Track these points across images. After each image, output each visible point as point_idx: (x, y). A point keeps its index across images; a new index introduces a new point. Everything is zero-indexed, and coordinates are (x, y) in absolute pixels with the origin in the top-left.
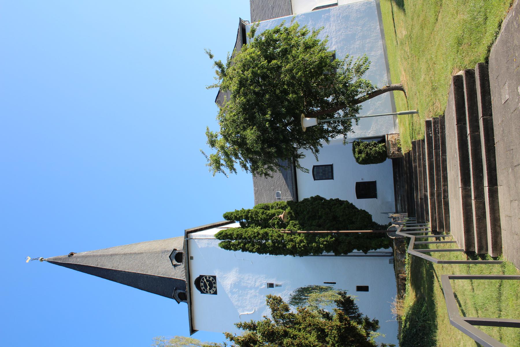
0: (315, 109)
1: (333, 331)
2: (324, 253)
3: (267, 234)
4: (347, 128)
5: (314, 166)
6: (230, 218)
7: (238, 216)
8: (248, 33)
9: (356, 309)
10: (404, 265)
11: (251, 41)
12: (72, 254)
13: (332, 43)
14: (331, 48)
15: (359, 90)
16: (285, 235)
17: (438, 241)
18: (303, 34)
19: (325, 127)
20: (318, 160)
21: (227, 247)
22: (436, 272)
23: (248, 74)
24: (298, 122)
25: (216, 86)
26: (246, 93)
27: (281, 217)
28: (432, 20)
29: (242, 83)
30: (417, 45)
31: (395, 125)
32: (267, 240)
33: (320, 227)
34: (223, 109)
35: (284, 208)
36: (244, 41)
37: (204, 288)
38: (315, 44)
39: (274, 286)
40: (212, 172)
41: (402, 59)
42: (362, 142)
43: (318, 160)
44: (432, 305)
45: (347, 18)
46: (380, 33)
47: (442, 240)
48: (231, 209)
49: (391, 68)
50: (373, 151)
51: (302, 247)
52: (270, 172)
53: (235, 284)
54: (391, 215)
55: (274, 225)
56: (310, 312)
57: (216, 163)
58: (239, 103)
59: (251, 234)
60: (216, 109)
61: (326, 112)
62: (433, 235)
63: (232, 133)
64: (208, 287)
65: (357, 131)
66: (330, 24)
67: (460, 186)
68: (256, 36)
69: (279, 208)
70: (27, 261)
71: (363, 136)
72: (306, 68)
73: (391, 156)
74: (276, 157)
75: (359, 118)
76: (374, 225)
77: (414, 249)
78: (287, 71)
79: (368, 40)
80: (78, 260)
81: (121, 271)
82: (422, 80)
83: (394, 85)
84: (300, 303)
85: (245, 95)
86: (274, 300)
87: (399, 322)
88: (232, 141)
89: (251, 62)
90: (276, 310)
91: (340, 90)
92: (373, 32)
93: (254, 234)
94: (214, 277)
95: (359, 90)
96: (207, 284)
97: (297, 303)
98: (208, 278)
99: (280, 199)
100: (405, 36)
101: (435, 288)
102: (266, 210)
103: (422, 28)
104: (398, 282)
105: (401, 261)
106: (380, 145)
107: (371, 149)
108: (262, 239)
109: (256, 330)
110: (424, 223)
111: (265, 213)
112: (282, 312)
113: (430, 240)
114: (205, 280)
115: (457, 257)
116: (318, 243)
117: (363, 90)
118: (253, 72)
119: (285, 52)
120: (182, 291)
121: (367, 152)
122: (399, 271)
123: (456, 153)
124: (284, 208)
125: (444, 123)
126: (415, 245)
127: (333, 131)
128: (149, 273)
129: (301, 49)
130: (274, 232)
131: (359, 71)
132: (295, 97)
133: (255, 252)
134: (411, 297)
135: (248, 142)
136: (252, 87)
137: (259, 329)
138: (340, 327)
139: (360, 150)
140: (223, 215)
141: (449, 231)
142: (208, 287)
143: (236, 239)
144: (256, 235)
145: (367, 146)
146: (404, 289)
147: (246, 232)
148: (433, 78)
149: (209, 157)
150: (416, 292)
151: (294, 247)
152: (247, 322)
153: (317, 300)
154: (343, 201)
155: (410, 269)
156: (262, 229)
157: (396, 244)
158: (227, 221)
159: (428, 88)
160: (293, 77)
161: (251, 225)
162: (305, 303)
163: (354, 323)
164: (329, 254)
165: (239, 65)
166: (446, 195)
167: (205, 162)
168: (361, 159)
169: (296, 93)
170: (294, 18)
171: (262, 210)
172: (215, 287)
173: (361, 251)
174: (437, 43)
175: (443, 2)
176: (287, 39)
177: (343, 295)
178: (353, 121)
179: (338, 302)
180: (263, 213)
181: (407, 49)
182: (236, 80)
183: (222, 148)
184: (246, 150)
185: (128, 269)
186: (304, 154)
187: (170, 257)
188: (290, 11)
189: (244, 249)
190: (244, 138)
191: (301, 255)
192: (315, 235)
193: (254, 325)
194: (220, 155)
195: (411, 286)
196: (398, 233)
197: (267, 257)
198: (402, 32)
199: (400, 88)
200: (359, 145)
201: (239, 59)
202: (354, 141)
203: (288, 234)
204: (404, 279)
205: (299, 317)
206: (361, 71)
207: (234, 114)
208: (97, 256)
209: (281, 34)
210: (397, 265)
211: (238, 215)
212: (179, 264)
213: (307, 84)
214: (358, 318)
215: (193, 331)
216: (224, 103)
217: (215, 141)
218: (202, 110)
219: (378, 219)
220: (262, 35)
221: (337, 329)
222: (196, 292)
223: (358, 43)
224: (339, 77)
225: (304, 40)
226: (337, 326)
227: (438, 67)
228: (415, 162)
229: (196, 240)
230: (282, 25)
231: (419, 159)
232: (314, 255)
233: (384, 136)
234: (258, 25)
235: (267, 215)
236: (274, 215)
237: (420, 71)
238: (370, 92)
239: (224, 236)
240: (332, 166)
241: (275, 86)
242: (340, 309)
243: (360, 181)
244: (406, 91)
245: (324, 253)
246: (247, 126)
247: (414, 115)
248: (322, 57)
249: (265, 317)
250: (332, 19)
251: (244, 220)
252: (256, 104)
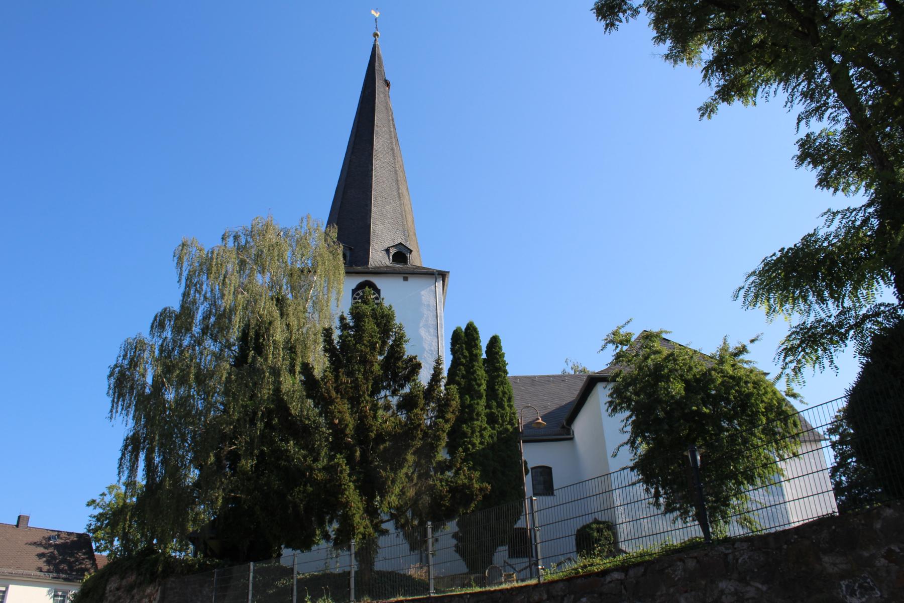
21: (456, 337)
70: (373, 12)
80: (382, 96)
81: (372, 164)
151: (465, 435)
222: (355, 281)
229: (433, 287)
235: (502, 400)
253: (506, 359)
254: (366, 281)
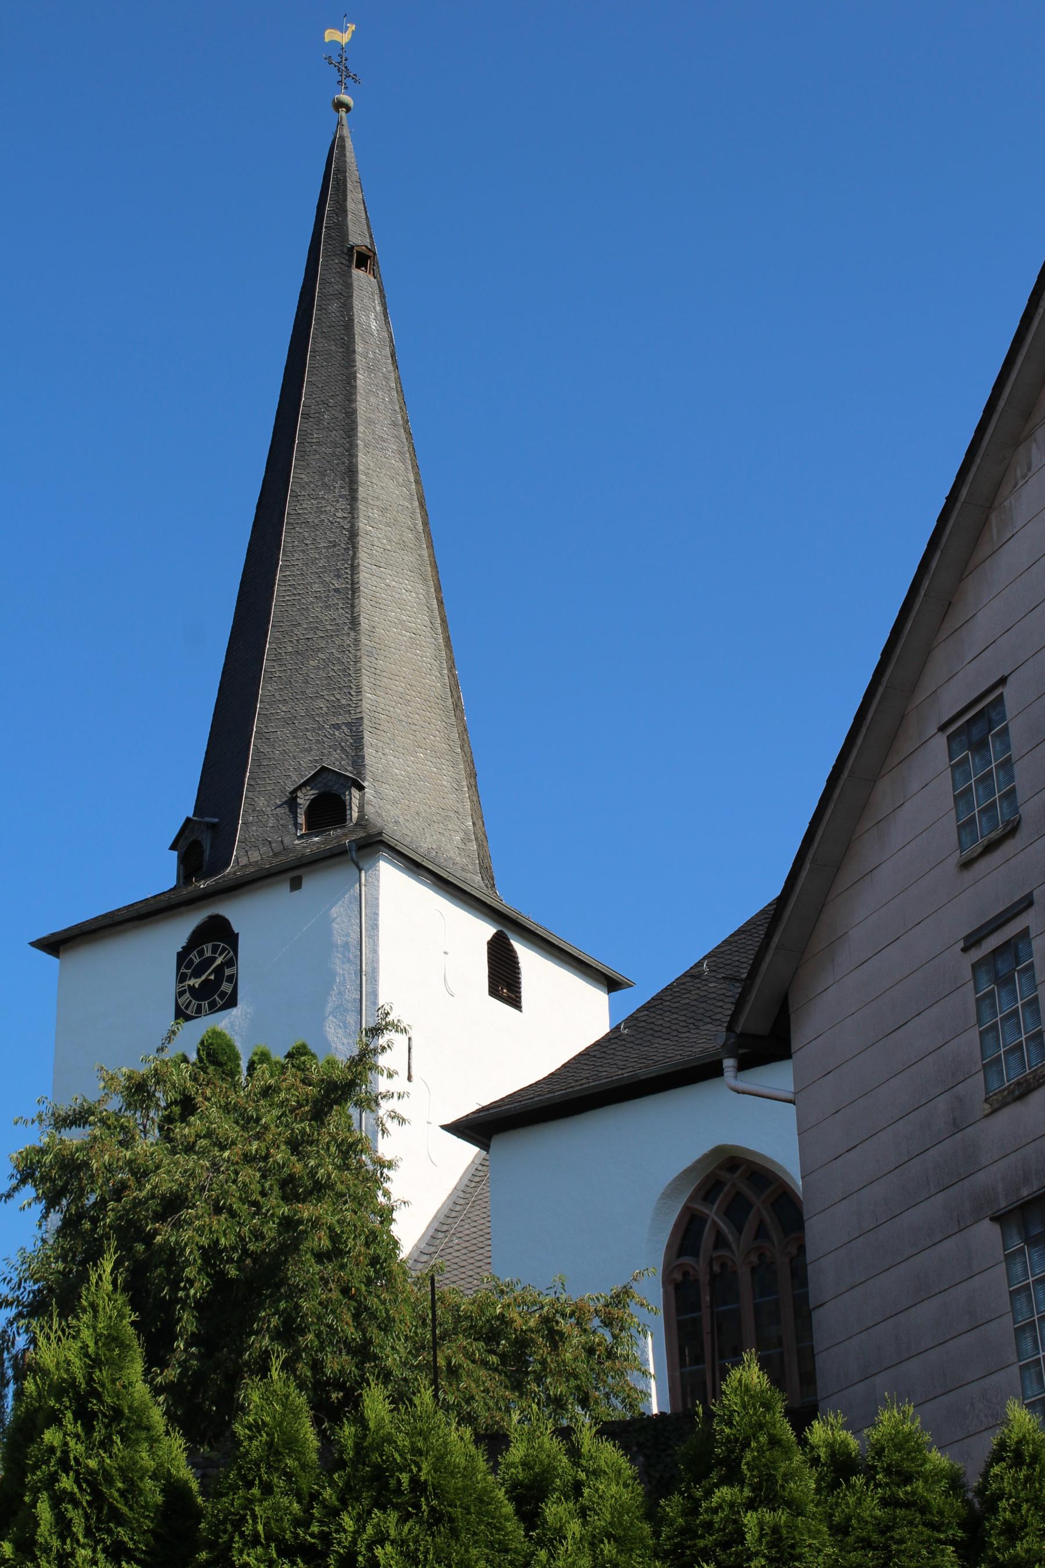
37: (197, 961)
98: (228, 972)
172: (199, 1010)
175: (585, 1562)
185: (285, 580)
212: (302, 819)
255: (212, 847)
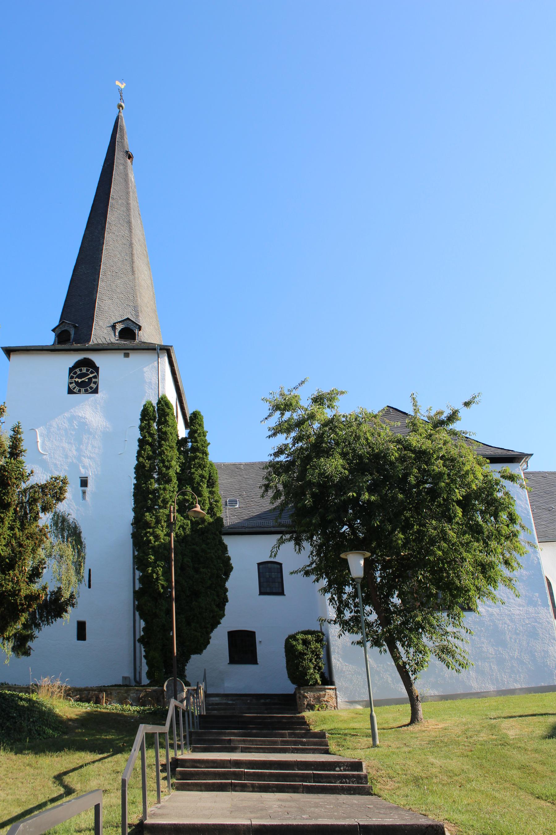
0: (378, 574)
1: (10, 584)
2: (138, 574)
3: (169, 481)
4: (346, 625)
5: (280, 564)
6: (193, 421)
7: (196, 435)
8: (509, 468)
9: (48, 621)
10: (121, 702)
11: (495, 471)
12: (130, 157)
13: (490, 606)
14: (483, 607)
15: (412, 650)
16: (167, 512)
17: (160, 768)
18: (507, 563)
19: (348, 589)
20: (291, 573)
21: (145, 414)
22: (110, 759)
23: (438, 466)
24: (357, 545)
25: (416, 411)
26: (405, 461)
27: (196, 507)
28: (538, 788)
29: (422, 456)
30: (490, 755)
31: (352, 702)
32: (158, 481)
33: (181, 569)
34: (378, 420)
35: (211, 511)
36: (494, 460)
38: (491, 580)
39: (83, 488)
40: (271, 396)
41: (465, 724)
42: (322, 647)
43: (291, 573)
44: (56, 747)
45: (533, 634)
46: (508, 688)
47: (163, 775)
48: (208, 425)
49: (448, 703)
50: (307, 664)
51: (148, 537)
52: (271, 493)
53: (85, 424)
54: (202, 686)
55: (184, 494)
56: (42, 546)
57: (286, 405)
58: (388, 449)
59: (167, 454)
60: (375, 407)
61: (372, 594)
62: (170, 760)
63: (337, 434)
64: (80, 380)
65: (340, 642)
66: (523, 606)
67: (253, 823)
68: (504, 482)
69: (211, 504)
70: (118, 83)
71: (332, 649)
72: (449, 563)
73: (300, 693)
74: (295, 507)
75: (365, 646)
76: (184, 658)
77: (146, 733)
78: (443, 532)
79: (495, 667)
80: (121, 167)
82: (432, 759)
83: (421, 707)
84: (57, 529)
85: (402, 459)
86: (61, 489)
87: (28, 688)
88: (323, 434)
89: (459, 472)
90: (43, 491)
91: (411, 617)
92: (510, 677)
93: (168, 461)
94: (96, 391)
95: (412, 650)
96: (84, 379)
97: (56, 524)
98: (94, 380)
99: (226, 505)
100: (506, 734)
101: (83, 754)
102: (208, 482)
103: (522, 768)
104: (92, 689)
105: (127, 698)
106: (318, 676)
107: (311, 660)
108: (160, 473)
109: (10, 458)
110: (190, 744)
111: (202, 481)
112: (40, 501)
113: (162, 752)
114: (91, 376)
115: (133, 803)
116: (154, 565)
117: (411, 656)
118: (441, 475)
119: (476, 531)
120: (72, 336)
121: (306, 654)
122: (111, 694)
123: (310, 818)
124: (211, 511)
125: (359, 794)
126: (153, 734)
127: (341, 601)
128: (101, 284)
129: (482, 557)
130: (171, 492)
131: (445, 651)
132: (398, 544)
133: (138, 460)
134: (68, 709)
135: (322, 460)
136: (416, 471)
137: (11, 463)
138: (17, 595)
139: (310, 643)
140: (198, 410)
141: (178, 789)
142: (80, 380)
143: (159, 430)
144: (166, 463)
145: (316, 655)
146: (80, 700)
147: (171, 447)
148: (435, 780)
149: (295, 393)
150: (76, 719)
151: (147, 525)
152: (23, 443)
153: (61, 556)
154: (223, 610)
155: (114, 711)
156: (177, 473)
157: (154, 691)
158: (188, 416)
159: (417, 771)
160: (433, 542)
161: (182, 457)
162: (57, 536)
163: (24, 618)
164: (137, 582)
165: (454, 452)
166: (237, 788)
167: (287, 387)
168: (294, 643)
169: (404, 546)
170: (533, 546)
171: (206, 475)
172: (80, 391)
173: (142, 633)
174: (497, 795)
176: (498, 535)
177: (71, 601)
178: (358, 637)
179: (58, 593)
180: (202, 476)
181: (483, 736)
182: (428, 445)
183: (312, 417)
184: (308, 455)
185: (106, 249)
186: (302, 551)
187: (128, 319)
188: (545, 538)
189: (142, 443)
190: (328, 453)
191: (134, 535)
192: (168, 560)
193: (18, 455)
194: (299, 412)
195: (87, 713)
196: (173, 703)
197: (131, 480)
198: (512, 730)
199: (414, 718)
200: (317, 641)
201: (463, 452)
202: (323, 634)
203: (169, 516)
204: (98, 701)
205: (33, 529)
206: (444, 656)
207: (370, 438)
208: (128, 198)
209: (508, 526)
210: (121, 690)
211: (199, 435)
212: (117, 334)
213: (423, 564)
214: (32, 624)
215: (9, 351)
216: (387, 421)
217: (322, 404)
218: (374, 385)
219: (195, 664)
220: (507, 494)
221: (15, 591)
222: (72, 359)
223: (491, 650)
224: (434, 618)
225: (497, 562)
226: (20, 590)
227: (456, 792)
228: (290, 735)
229: (156, 363)
230: (523, 528)
231: (295, 743)
232: (134, 557)
233: (332, 683)
234: (522, 486)
235: (198, 484)
236: (200, 495)
237: (446, 757)
238: (407, 667)
239: (163, 410)
240: (282, 593)
241: (417, 509)
242: (46, 595)
243: (258, 639)
244: (410, 728)
245: (138, 574)
246: (348, 459)
247: (370, 739)
248: (468, 591)
249: (32, 472)
250: (531, 609)
251: (190, 444)
252: (387, 478)
253: (209, 438)
254: (85, 358)
255: (74, 334)
